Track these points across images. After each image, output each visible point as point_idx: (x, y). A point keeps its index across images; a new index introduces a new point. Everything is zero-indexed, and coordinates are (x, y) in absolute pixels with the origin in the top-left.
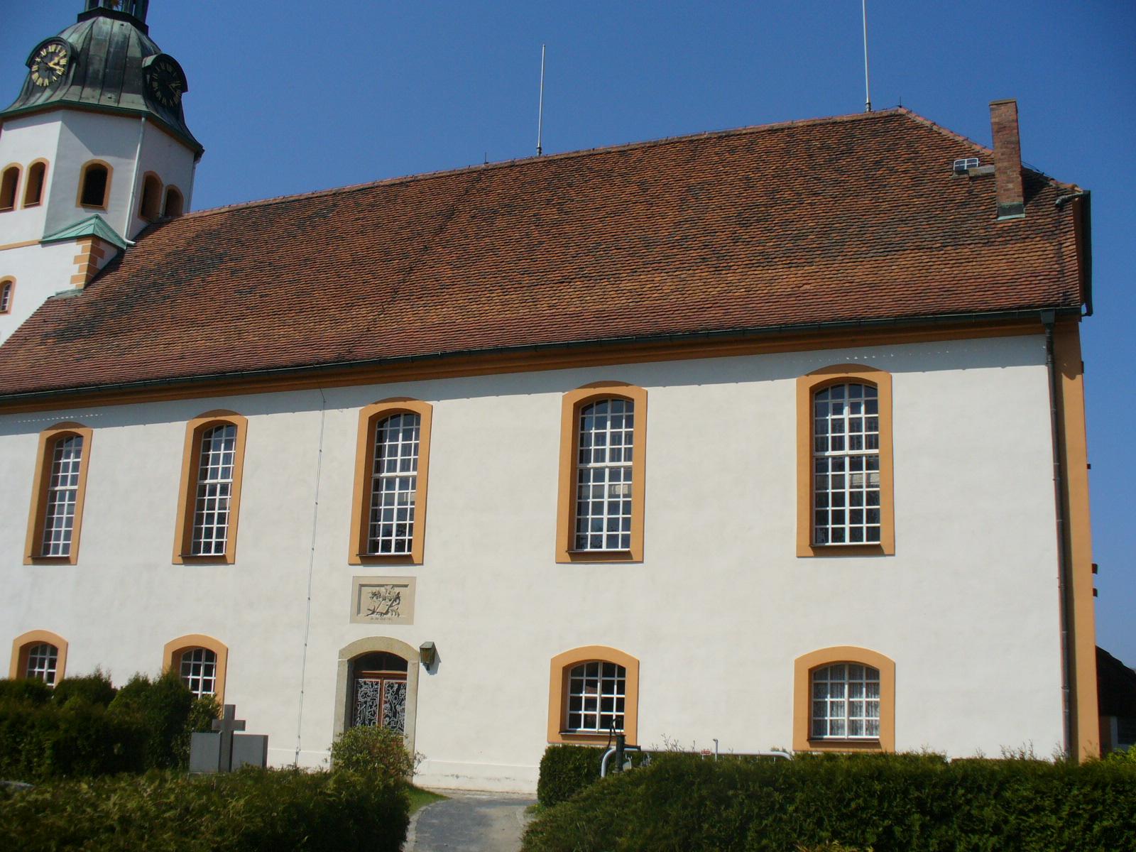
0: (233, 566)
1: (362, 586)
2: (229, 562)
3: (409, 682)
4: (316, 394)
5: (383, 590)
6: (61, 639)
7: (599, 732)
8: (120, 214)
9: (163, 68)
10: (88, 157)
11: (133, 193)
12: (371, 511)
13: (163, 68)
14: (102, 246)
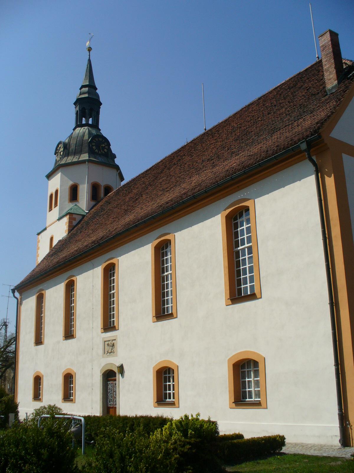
1: (105, 341)
2: (258, 297)
3: (117, 382)
4: (89, 264)
5: (110, 342)
6: (259, 355)
7: (172, 401)
8: (84, 202)
9: (97, 140)
10: (71, 183)
11: (87, 192)
13: (97, 140)
14: (74, 216)
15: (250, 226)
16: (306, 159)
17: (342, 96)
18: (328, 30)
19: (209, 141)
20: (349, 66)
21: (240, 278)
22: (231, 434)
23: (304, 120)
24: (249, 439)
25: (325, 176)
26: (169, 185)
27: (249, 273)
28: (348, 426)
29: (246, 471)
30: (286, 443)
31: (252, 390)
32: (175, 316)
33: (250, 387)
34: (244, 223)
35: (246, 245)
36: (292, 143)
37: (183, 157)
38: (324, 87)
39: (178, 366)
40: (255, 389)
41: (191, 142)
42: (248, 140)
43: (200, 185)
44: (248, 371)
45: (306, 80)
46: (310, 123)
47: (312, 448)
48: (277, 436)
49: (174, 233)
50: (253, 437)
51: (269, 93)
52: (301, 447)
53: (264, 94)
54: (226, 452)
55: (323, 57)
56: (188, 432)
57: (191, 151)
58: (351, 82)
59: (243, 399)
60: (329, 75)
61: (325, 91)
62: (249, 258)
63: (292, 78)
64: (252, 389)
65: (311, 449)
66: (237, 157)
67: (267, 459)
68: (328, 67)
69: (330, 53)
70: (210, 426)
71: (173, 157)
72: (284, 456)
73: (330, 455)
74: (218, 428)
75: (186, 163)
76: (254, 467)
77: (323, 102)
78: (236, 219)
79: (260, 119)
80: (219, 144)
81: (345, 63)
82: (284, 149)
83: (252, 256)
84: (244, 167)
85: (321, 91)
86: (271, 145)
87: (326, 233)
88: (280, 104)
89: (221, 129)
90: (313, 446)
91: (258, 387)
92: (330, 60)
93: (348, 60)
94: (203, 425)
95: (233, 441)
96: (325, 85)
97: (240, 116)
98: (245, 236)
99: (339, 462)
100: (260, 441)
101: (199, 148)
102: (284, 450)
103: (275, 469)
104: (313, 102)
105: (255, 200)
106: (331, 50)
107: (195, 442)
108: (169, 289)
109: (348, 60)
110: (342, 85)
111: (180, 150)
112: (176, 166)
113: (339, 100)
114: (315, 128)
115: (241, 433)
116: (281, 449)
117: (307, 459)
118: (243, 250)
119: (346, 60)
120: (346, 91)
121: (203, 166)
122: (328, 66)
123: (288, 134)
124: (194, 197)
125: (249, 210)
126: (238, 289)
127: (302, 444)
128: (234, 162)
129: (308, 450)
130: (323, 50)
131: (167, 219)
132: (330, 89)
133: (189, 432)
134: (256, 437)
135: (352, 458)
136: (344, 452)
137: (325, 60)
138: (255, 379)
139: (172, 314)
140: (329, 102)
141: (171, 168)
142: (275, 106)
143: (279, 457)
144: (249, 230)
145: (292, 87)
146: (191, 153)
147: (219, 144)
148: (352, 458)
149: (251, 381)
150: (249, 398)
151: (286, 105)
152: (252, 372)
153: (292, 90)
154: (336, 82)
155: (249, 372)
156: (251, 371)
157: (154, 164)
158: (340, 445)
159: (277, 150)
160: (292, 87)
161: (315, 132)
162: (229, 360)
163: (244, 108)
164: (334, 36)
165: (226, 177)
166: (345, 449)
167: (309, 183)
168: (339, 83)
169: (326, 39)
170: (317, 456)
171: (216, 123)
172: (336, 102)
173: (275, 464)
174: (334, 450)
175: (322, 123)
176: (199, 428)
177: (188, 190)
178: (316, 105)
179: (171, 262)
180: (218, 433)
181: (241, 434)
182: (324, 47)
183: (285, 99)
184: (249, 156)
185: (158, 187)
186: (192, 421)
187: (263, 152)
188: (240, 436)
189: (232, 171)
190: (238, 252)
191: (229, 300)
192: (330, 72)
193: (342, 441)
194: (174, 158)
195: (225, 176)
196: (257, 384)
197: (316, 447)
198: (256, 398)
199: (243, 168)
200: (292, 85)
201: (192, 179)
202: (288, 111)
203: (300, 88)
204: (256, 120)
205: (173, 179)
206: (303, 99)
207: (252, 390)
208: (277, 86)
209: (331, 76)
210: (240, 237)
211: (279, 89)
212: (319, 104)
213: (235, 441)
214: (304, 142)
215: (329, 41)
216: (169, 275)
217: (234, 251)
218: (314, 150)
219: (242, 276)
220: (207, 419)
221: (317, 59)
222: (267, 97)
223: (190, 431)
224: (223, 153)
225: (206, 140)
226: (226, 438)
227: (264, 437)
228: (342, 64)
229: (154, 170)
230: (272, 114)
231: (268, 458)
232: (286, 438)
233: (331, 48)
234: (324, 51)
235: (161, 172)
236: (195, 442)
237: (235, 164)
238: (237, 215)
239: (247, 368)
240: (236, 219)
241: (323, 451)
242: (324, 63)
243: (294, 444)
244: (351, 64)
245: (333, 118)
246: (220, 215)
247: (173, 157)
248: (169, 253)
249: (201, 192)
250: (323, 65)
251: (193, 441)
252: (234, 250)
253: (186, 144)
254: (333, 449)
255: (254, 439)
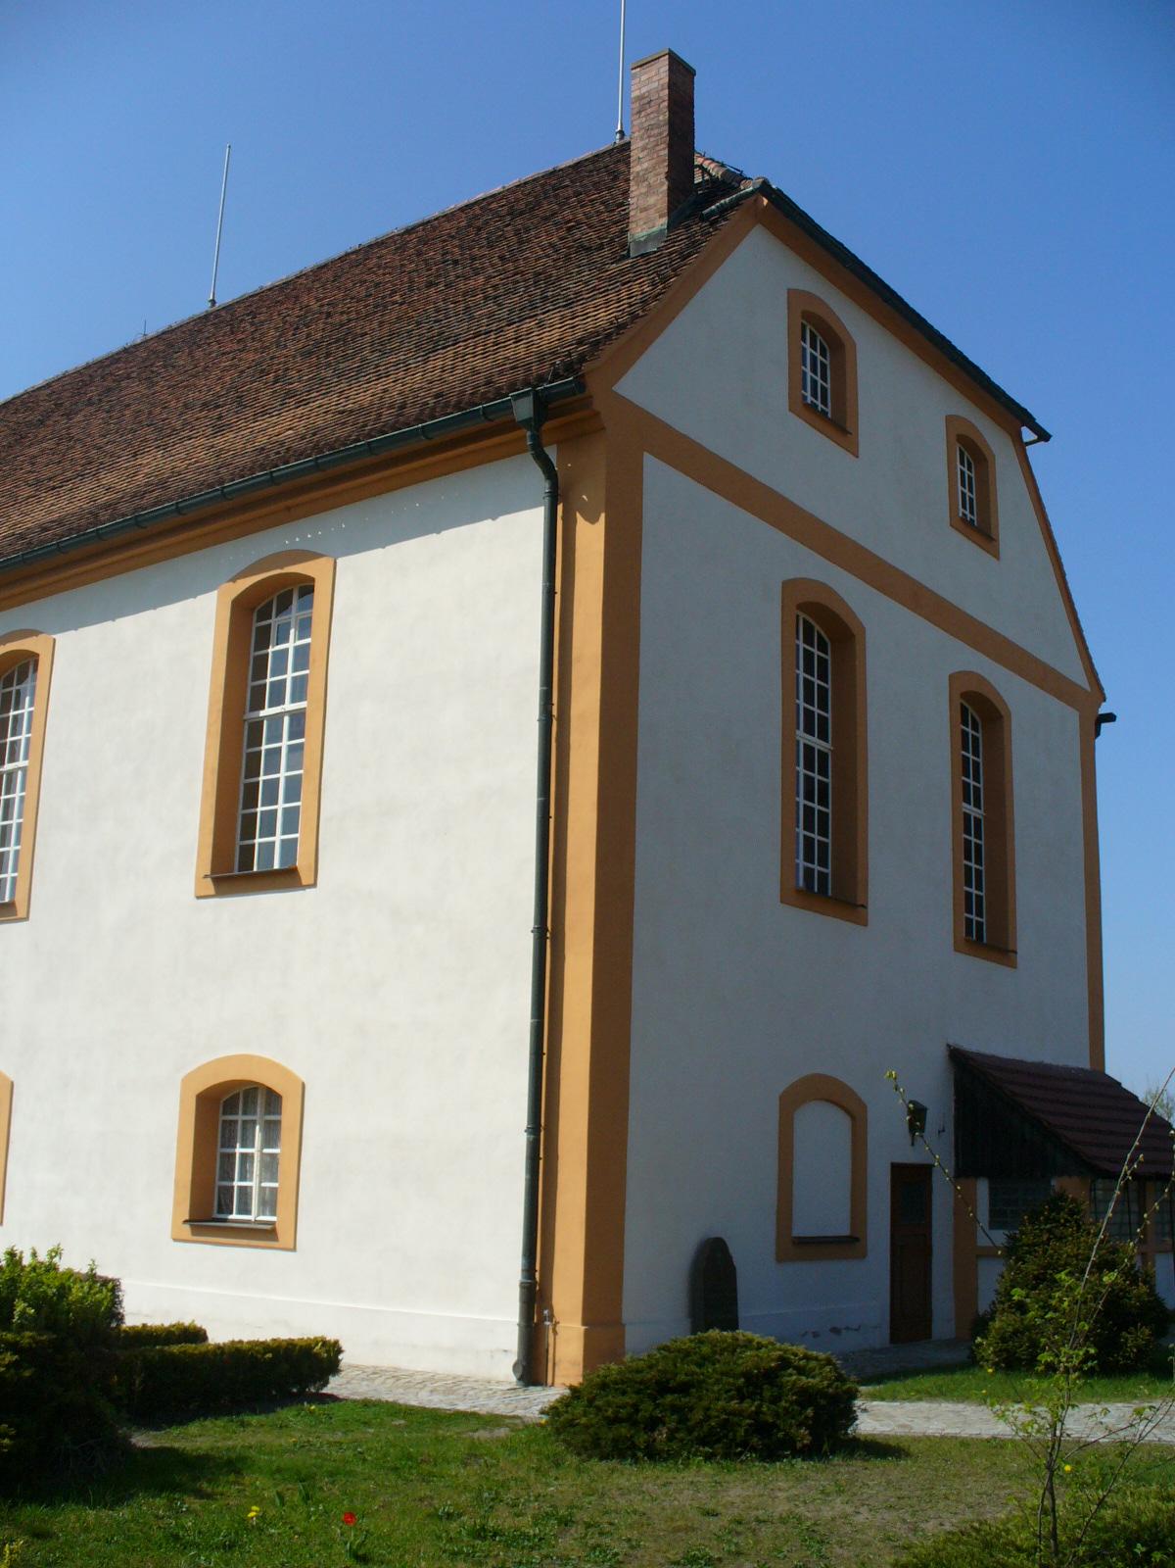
0: (313, 890)
2: (304, 882)
6: (287, 1074)
12: (242, 788)
15: (308, 645)
16: (525, 451)
17: (674, 270)
18: (667, 51)
19: (218, 342)
20: (713, 180)
21: (253, 810)
22: (167, 1324)
23: (540, 325)
24: (224, 1344)
25: (578, 515)
26: (57, 469)
27: (286, 801)
28: (547, 1323)
29: (199, 1448)
30: (342, 1365)
31: (251, 1187)
32: (21, 913)
33: (248, 1176)
34: (292, 631)
35: (289, 706)
36: (489, 392)
37: (123, 384)
38: (624, 232)
39: (12, 1084)
40: (263, 1185)
41: (159, 337)
42: (345, 358)
43: (163, 484)
44: (245, 1122)
45: (570, 198)
46: (557, 337)
47: (425, 1386)
48: (316, 1341)
49: (55, 633)
50: (237, 1339)
51: (443, 217)
52: (391, 1381)
53: (427, 218)
54: (137, 1382)
55: (636, 134)
56: (12, 1308)
57: (151, 365)
58: (711, 230)
59: (220, 1211)
60: (647, 194)
61: (624, 246)
62: (291, 749)
63: (526, 183)
64: (253, 1184)
65: (421, 1389)
66: (299, 411)
67: (274, 1411)
68: (646, 169)
69: (659, 127)
70: (92, 1292)
71: (90, 376)
72: (332, 1405)
73: (476, 1409)
74: (121, 1302)
75: (129, 405)
76: (228, 1434)
77: (610, 278)
78: (265, 614)
79: (397, 298)
80: (251, 357)
81: (701, 167)
82: (458, 407)
83: (302, 744)
84: (317, 448)
85: (612, 240)
86: (421, 388)
87: (555, 700)
88: (473, 259)
89: (264, 310)
90: (428, 1380)
91: (274, 1179)
92: (658, 148)
93: (713, 161)
94: (70, 1289)
95: (166, 1348)
96: (627, 226)
97: (336, 278)
98: (289, 676)
99: (502, 1430)
100: (258, 1352)
101: (182, 362)
102: (334, 1386)
103: (295, 1444)
104: (579, 273)
105: (339, 561)
106: (664, 117)
107: (37, 1343)
108: (12, 819)
109: (713, 161)
110: (679, 235)
111: (116, 357)
112: (92, 409)
113: (665, 280)
114: (569, 355)
115: (199, 1324)
116: (326, 1383)
117: (404, 1418)
118: (276, 719)
119: (707, 159)
120: (689, 255)
121: (186, 423)
122: (645, 165)
123: (478, 363)
124: (137, 522)
125: (313, 591)
126: (241, 847)
127: (396, 1370)
128: (286, 427)
129: (412, 1390)
130: (639, 112)
131: (16, 590)
132: (642, 239)
133: (18, 1310)
134: (245, 1340)
135: (544, 1419)
136: (523, 1402)
137: (641, 144)
138: (266, 1151)
139: (11, 906)
140: (629, 282)
141: (77, 414)
142: (456, 262)
143: (313, 1407)
144: (303, 656)
145: (522, 213)
146: (153, 372)
147: (251, 357)
148: (544, 1419)
149: (252, 1155)
150: (240, 1212)
151: (492, 266)
152: (258, 1128)
153: (519, 221)
154: (662, 222)
155: (248, 1126)
156: (254, 1123)
157: (21, 391)
158: (514, 1379)
159: (433, 409)
160: (522, 213)
161: (570, 368)
162: (186, 1081)
163: (353, 253)
164: (681, 76)
165: (252, 470)
166: (527, 1392)
167: (525, 529)
168: (671, 226)
169: (655, 78)
170: (439, 1409)
171: (250, 287)
172: (654, 285)
173: (299, 1430)
174: (495, 1393)
175: (596, 342)
176: (52, 1297)
177: (120, 495)
178: (586, 283)
179: (29, 731)
180: (120, 1318)
181: (199, 1325)
182: (646, 101)
183: (491, 246)
184: (343, 412)
185: (21, 469)
186: (30, 1272)
187: (390, 408)
188: (196, 1335)
189: (278, 453)
190: (256, 727)
191: (209, 880)
192: (649, 186)
193: (520, 1368)
194: (92, 381)
195: (252, 468)
196: (271, 1166)
197: (439, 1384)
198: (264, 1214)
199: (313, 448)
200: (521, 206)
201: (139, 462)
202: (495, 287)
203: (546, 219)
204: (383, 298)
205: (77, 453)
206: (547, 256)
207: (251, 1187)
208: (473, 200)
209: (652, 200)
210: (273, 676)
211: (478, 212)
212: (596, 283)
213: (175, 1349)
214: (526, 394)
215: (662, 85)
216: (20, 773)
217: (245, 720)
218: (553, 425)
219: (263, 805)
220: (82, 1268)
221: (618, 136)
222: (434, 229)
223: (20, 1306)
224: (257, 391)
225: (208, 338)
226: (147, 1337)
227: (274, 1340)
228: (691, 166)
229: (16, 411)
230: (441, 287)
231: (279, 1409)
232: (343, 1349)
233: (666, 110)
234: (643, 114)
235: (42, 422)
236: (37, 1343)
237: (291, 432)
238: (270, 604)
239: (245, 1113)
240: (266, 614)
241: (459, 1394)
242: (635, 154)
243: (370, 1371)
244: (720, 173)
245: (632, 332)
246: (215, 594)
247: (90, 376)
248: (27, 699)
249: (163, 508)
250: (632, 159)
251: (27, 1341)
252: (245, 718)
253: (139, 341)
254: (490, 1392)
255: (239, 1346)
